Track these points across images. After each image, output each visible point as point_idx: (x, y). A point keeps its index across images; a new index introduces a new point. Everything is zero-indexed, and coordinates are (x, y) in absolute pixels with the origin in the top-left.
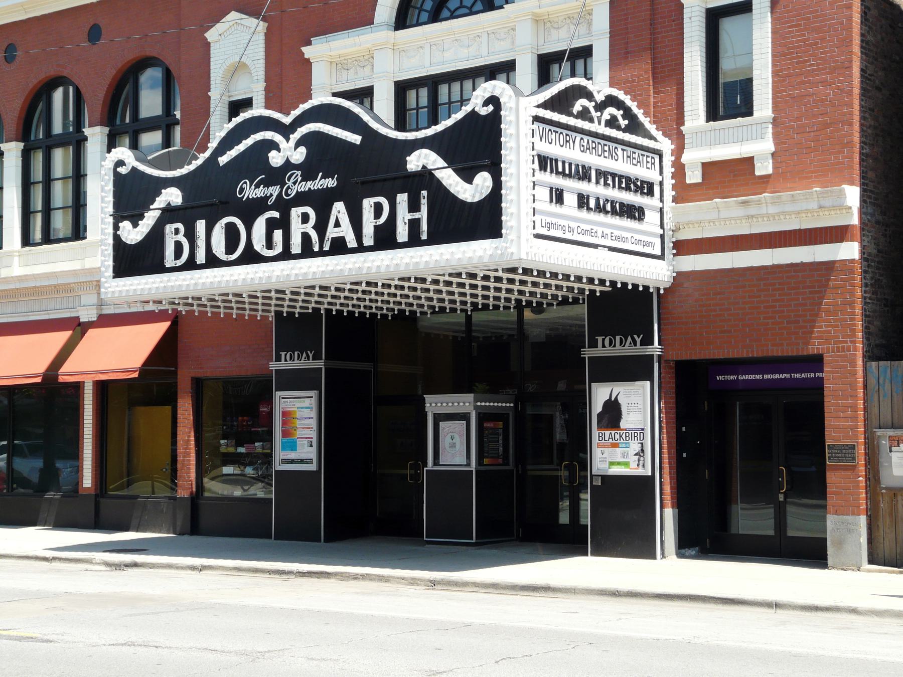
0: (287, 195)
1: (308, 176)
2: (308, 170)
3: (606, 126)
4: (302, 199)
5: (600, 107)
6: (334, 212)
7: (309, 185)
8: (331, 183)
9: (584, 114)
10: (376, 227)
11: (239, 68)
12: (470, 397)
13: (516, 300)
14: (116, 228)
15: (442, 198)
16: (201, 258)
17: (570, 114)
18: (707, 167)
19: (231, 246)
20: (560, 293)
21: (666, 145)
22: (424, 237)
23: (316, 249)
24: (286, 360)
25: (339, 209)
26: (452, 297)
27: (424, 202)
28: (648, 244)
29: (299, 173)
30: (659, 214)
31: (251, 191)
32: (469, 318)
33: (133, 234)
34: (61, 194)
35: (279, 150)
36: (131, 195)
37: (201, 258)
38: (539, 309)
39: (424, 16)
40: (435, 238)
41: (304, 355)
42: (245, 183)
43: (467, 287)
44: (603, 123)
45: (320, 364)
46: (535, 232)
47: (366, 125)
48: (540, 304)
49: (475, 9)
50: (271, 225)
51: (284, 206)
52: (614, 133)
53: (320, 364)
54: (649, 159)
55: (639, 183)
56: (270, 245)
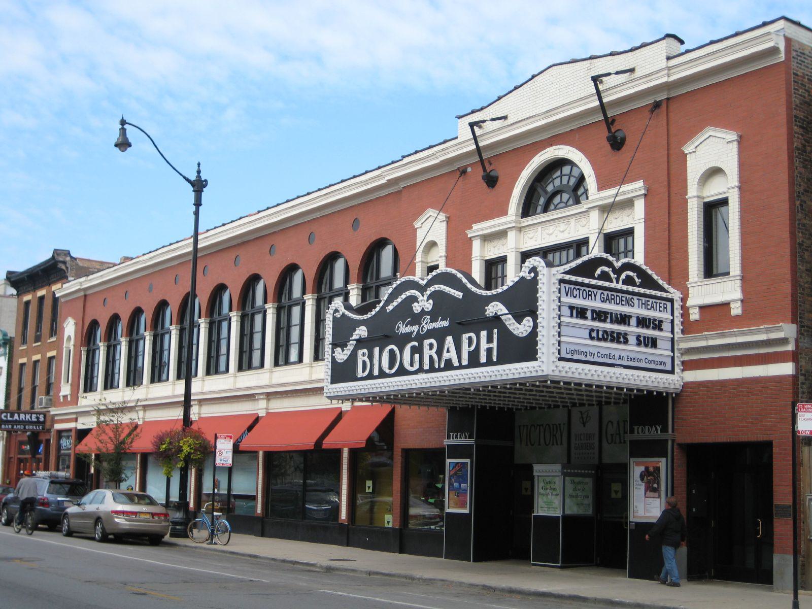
0: (422, 331)
1: (433, 320)
2: (434, 315)
4: (430, 334)
6: (447, 342)
8: (445, 323)
9: (605, 276)
10: (469, 353)
11: (716, 171)
13: (624, 399)
14: (333, 352)
15: (506, 336)
16: (376, 372)
17: (594, 278)
18: (702, 308)
21: (676, 295)
22: (495, 359)
23: (437, 366)
25: (449, 339)
27: (495, 336)
29: (429, 317)
31: (403, 329)
33: (342, 355)
37: (376, 372)
40: (502, 361)
42: (400, 323)
44: (621, 281)
45: (471, 442)
47: (464, 286)
49: (568, 204)
50: (414, 351)
51: (420, 338)
52: (631, 288)
55: (657, 323)
56: (412, 365)
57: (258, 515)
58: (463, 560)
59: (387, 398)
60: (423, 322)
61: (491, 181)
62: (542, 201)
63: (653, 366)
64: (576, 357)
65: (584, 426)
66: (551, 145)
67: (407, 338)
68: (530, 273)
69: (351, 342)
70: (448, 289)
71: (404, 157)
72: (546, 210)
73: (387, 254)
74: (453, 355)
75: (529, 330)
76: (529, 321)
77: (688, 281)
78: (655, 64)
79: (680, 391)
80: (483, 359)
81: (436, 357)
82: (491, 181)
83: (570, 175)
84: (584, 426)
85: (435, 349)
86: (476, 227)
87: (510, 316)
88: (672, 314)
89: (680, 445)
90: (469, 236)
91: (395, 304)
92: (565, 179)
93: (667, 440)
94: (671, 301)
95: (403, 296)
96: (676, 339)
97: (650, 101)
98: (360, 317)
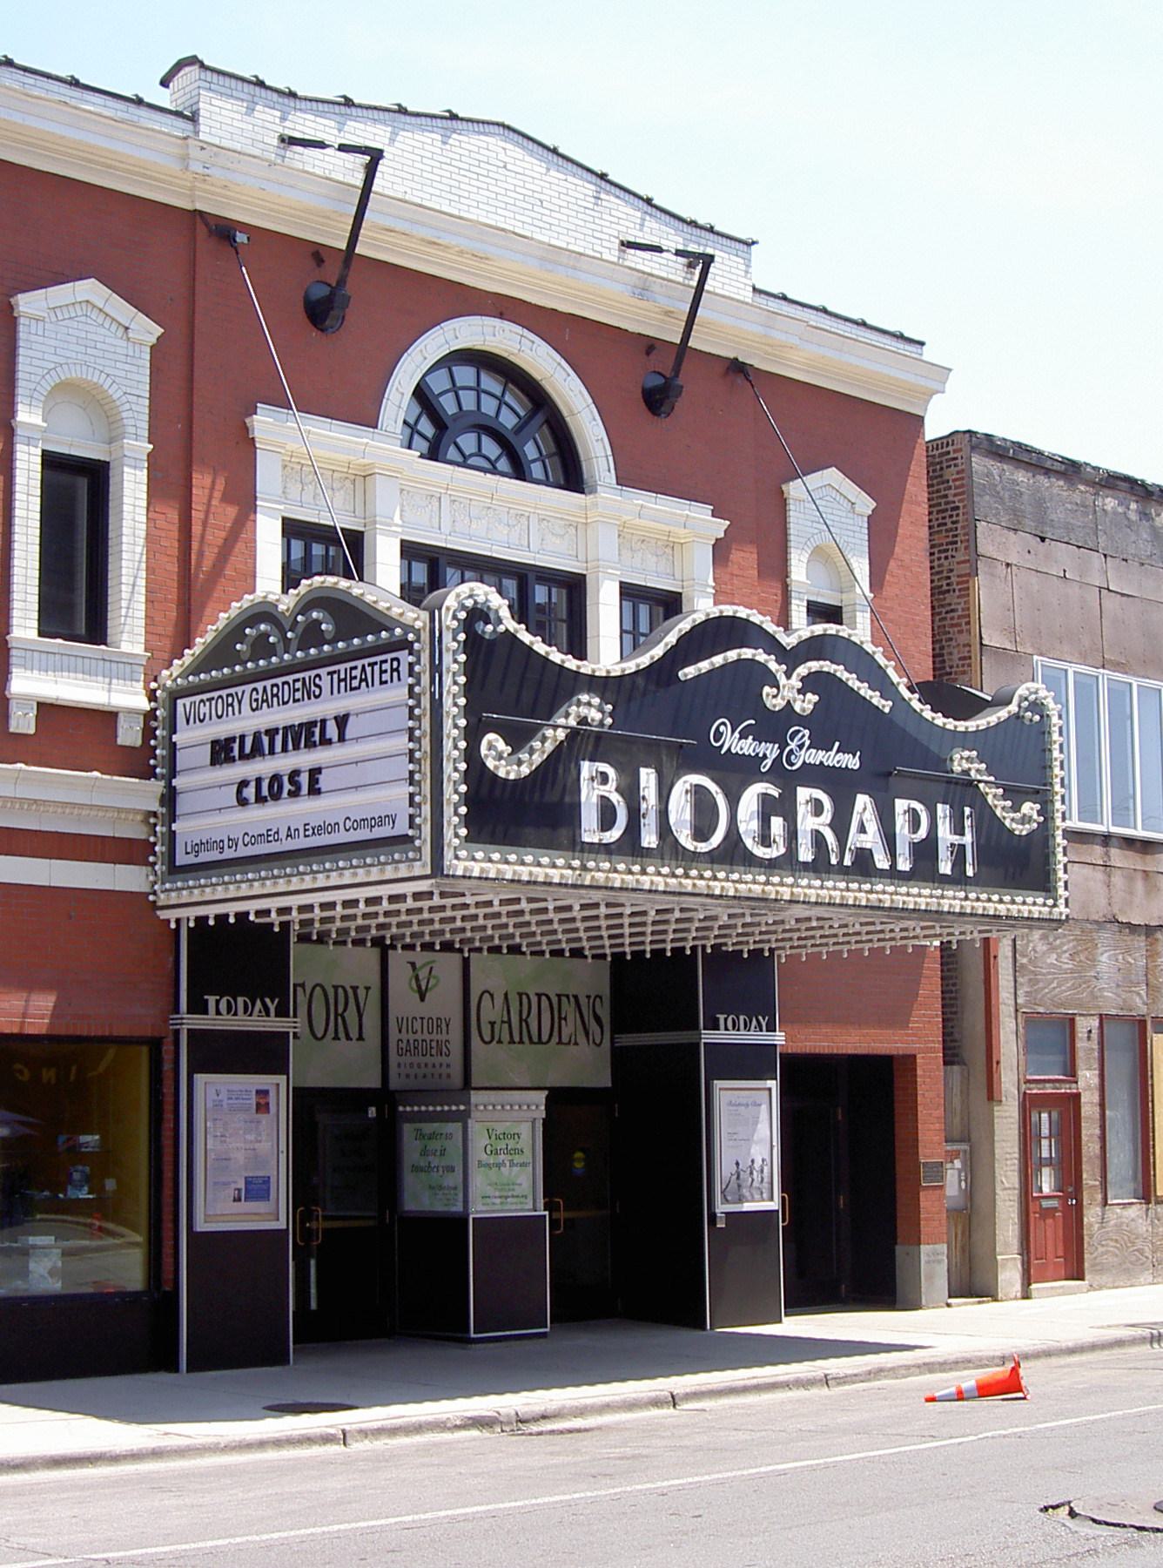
2: (824, 731)
4: (816, 775)
6: (858, 807)
8: (852, 762)
16: (649, 839)
23: (834, 861)
29: (807, 732)
31: (734, 742)
45: (708, 1037)
50: (768, 808)
51: (787, 778)
56: (765, 839)
58: (225, 1368)
65: (422, 999)
74: (871, 839)
80: (945, 868)
84: (422, 999)
85: (827, 816)
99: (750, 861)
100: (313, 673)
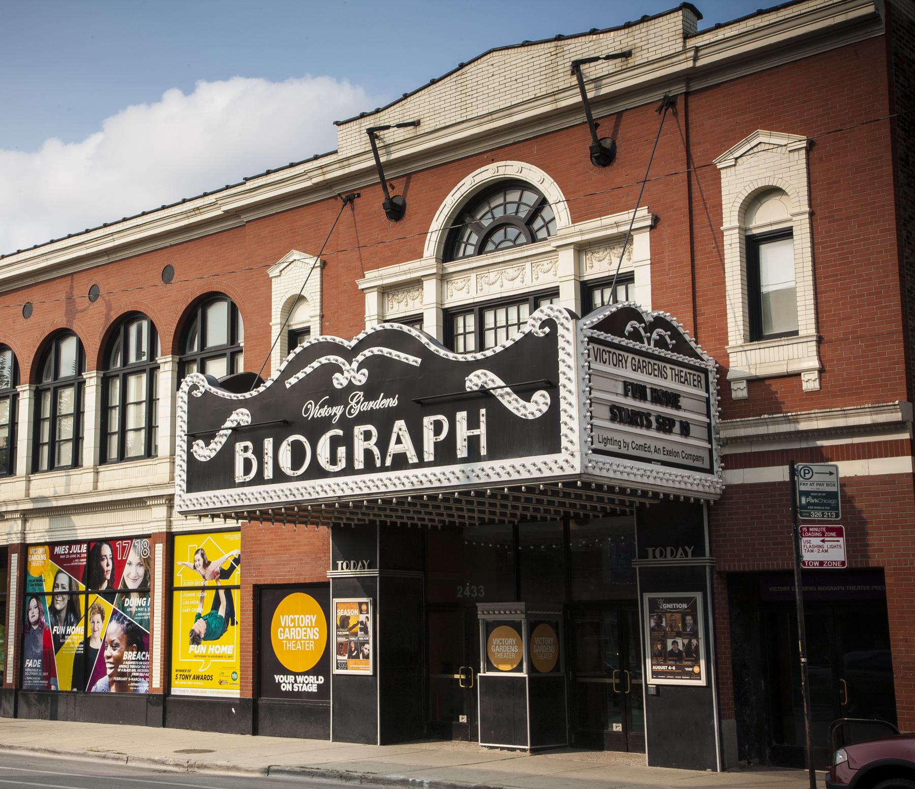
0: (350, 414)
2: (370, 391)
3: (655, 346)
4: (364, 417)
5: (650, 328)
6: (395, 429)
7: (372, 405)
8: (392, 402)
9: (635, 335)
10: (436, 444)
11: (299, 299)
12: (521, 605)
14: (190, 446)
16: (268, 473)
17: (621, 334)
19: (297, 462)
20: (562, 510)
22: (483, 452)
24: (342, 569)
25: (400, 425)
26: (461, 513)
27: (483, 419)
28: (698, 458)
29: (362, 393)
30: (706, 430)
31: (315, 411)
32: (516, 529)
33: (204, 452)
34: (136, 417)
35: (342, 373)
36: (203, 419)
37: (268, 473)
38: (583, 520)
39: (470, 250)
40: (493, 455)
41: (360, 564)
43: (475, 503)
44: (652, 342)
45: (375, 573)
46: (594, 446)
48: (587, 516)
49: (517, 242)
50: (335, 442)
51: (347, 424)
52: (663, 353)
53: (375, 573)
54: (695, 378)
56: (333, 460)
57: (8, 687)
59: (314, 511)
60: (352, 400)
61: (396, 211)
62: (474, 239)
63: (689, 462)
64: (610, 447)
66: (493, 161)
67: (324, 424)
68: (541, 327)
69: (221, 432)
70: (395, 354)
71: (247, 179)
72: (481, 250)
73: (217, 316)
74: (407, 447)
75: (545, 409)
76: (544, 396)
77: (727, 344)
78: (664, 45)
79: (719, 497)
80: (462, 452)
81: (376, 452)
82: (396, 211)
83: (519, 203)
85: (374, 439)
86: (369, 274)
87: (508, 390)
88: (707, 391)
89: (719, 573)
90: (360, 287)
91: (301, 375)
92: (511, 209)
93: (705, 567)
94: (705, 371)
95: (316, 364)
96: (713, 424)
97: (657, 96)
98: (233, 395)
99: (324, 474)
100: (664, 364)
